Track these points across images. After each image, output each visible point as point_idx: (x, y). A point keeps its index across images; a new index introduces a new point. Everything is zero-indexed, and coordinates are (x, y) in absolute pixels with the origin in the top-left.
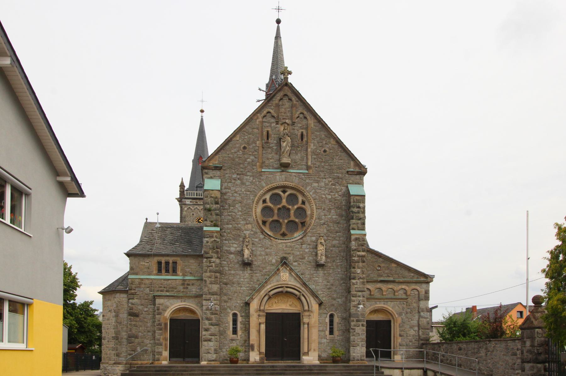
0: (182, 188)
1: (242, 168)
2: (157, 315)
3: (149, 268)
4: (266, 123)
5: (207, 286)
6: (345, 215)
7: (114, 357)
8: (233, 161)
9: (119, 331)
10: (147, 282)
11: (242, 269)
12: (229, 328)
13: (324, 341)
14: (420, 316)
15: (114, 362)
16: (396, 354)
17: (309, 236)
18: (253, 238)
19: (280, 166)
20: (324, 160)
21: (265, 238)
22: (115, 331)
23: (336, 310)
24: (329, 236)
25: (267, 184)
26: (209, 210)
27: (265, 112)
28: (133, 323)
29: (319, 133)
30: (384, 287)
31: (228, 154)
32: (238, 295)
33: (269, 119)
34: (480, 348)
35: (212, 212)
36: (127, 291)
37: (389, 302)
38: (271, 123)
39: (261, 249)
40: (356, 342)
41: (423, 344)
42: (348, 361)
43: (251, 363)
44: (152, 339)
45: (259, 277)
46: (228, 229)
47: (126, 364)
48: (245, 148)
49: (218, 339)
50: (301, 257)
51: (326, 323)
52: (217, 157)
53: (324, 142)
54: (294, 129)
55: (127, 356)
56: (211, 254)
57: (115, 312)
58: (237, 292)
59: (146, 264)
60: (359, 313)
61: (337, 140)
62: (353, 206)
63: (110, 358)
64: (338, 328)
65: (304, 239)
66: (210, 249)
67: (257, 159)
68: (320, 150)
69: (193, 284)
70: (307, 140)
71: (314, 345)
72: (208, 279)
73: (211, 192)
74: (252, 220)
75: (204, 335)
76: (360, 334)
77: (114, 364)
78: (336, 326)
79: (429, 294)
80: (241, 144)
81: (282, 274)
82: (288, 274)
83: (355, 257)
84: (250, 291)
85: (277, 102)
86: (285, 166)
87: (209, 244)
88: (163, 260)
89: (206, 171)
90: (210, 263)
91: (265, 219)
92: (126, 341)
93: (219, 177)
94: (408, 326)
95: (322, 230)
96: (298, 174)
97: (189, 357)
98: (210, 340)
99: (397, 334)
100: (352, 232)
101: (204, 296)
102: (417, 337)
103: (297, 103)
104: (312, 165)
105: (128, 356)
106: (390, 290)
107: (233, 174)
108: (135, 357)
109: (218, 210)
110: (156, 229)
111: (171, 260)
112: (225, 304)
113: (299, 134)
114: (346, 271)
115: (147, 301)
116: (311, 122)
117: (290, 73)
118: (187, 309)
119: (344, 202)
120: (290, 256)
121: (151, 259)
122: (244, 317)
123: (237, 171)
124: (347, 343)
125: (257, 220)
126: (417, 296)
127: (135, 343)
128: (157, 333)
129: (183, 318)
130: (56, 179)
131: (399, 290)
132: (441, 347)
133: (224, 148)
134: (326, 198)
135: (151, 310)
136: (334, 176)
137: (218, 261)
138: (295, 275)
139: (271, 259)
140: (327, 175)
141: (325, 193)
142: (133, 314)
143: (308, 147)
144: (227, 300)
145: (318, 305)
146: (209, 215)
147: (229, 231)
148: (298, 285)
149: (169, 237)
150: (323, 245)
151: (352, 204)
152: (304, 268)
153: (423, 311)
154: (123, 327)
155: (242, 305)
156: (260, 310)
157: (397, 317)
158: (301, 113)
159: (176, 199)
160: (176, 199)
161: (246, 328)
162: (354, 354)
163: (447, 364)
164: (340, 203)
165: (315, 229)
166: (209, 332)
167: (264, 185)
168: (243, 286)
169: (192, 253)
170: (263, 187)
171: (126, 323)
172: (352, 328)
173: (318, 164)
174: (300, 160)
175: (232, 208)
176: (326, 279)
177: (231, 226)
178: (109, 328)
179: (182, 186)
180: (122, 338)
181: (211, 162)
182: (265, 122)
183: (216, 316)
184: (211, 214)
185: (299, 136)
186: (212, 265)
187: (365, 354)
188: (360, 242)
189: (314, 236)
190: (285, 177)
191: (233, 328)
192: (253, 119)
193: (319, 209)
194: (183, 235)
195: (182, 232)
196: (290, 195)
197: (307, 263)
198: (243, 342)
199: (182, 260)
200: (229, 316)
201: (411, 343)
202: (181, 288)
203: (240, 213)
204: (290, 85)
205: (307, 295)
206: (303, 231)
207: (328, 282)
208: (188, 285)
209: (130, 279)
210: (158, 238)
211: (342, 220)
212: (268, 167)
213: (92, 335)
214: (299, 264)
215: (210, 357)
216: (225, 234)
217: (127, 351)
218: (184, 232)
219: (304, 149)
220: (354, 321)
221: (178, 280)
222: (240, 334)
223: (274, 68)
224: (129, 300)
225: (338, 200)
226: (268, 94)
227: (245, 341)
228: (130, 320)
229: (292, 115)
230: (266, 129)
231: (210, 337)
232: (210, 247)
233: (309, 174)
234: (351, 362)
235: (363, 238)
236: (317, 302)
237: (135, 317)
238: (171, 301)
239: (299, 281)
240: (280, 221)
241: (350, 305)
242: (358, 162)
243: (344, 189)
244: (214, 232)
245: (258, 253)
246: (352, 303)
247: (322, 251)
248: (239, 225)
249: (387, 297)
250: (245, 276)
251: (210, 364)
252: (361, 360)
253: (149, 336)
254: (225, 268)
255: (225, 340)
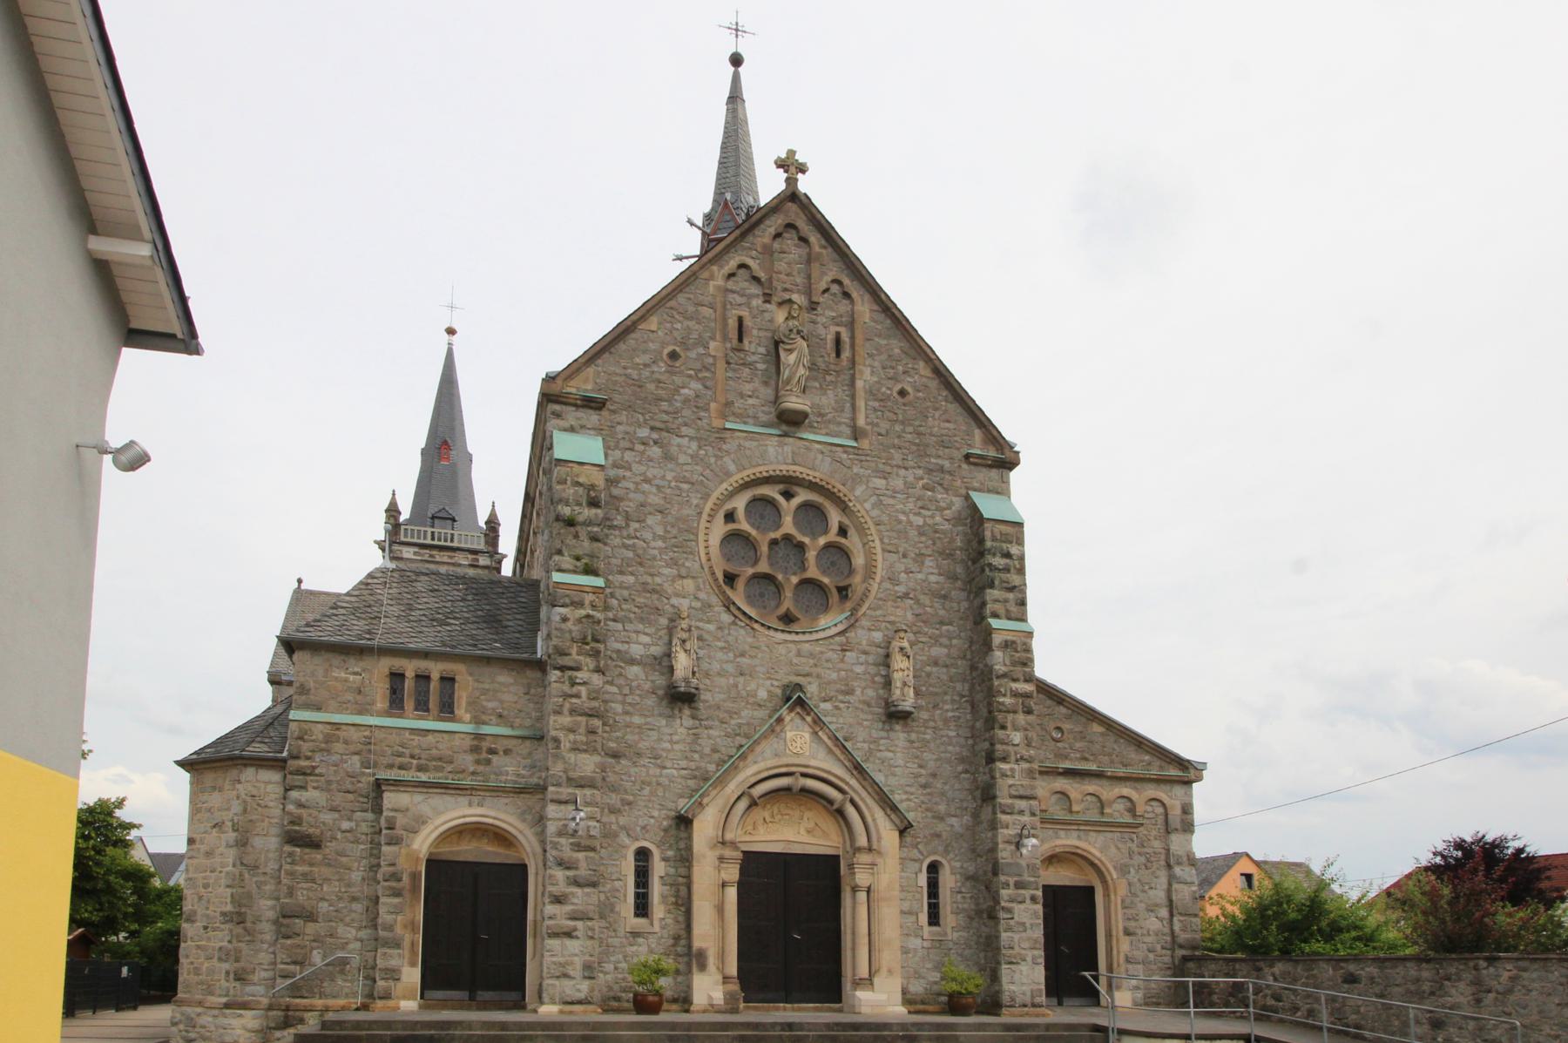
0: (393, 516)
1: (667, 413)
2: (389, 844)
3: (360, 692)
4: (735, 295)
5: (563, 758)
6: (963, 576)
7: (224, 984)
8: (639, 390)
9: (249, 895)
10: (355, 735)
11: (668, 711)
12: (625, 896)
13: (915, 943)
14: (1172, 879)
15: (224, 1000)
16: (1118, 988)
17: (863, 628)
18: (701, 620)
19: (776, 420)
20: (900, 417)
21: (736, 624)
22: (232, 895)
23: (946, 852)
24: (919, 632)
25: (741, 468)
26: (570, 523)
27: (732, 264)
28: (300, 869)
29: (884, 342)
30: (1074, 788)
31: (625, 368)
32: (653, 793)
33: (741, 282)
34: (1449, 979)
35: (578, 528)
36: (284, 761)
37: (1092, 834)
38: (750, 297)
39: (725, 657)
40: (1017, 949)
41: (1185, 959)
42: (993, 1005)
43: (698, 1012)
44: (364, 924)
45: (718, 740)
46: (621, 587)
47: (270, 1008)
48: (674, 356)
49: (596, 932)
50: (843, 688)
51: (919, 889)
52: (591, 370)
53: (900, 368)
54: (814, 322)
55: (275, 979)
56: (575, 656)
57: (234, 830)
58: (649, 784)
59: (351, 678)
60: (1023, 863)
61: (934, 365)
62: (993, 551)
63: (209, 986)
64: (955, 905)
65: (851, 635)
66: (573, 640)
67: (710, 393)
68: (888, 388)
69: (507, 752)
70: (854, 356)
71: (889, 957)
72: (566, 736)
73: (576, 468)
74: (697, 565)
75: (550, 918)
76: (1028, 925)
77: (227, 1006)
78: (948, 900)
79: (1192, 814)
80: (664, 344)
81: (789, 735)
82: (807, 736)
83: (1005, 695)
84: (691, 783)
85: (767, 240)
86: (791, 421)
87: (569, 625)
88: (410, 668)
89: (557, 407)
90: (573, 684)
91: (731, 569)
92: (274, 928)
93: (594, 429)
94: (1143, 905)
95: (899, 612)
96: (829, 448)
97: (488, 988)
98: (569, 934)
99: (1117, 927)
100: (995, 623)
101: (551, 789)
102: (1169, 938)
103: (824, 251)
104: (869, 428)
105: (279, 980)
106: (1089, 798)
107: (640, 426)
108: (302, 983)
109: (599, 525)
110: (381, 575)
111: (436, 669)
112: (613, 818)
113: (830, 338)
114: (972, 737)
115: (350, 796)
116: (864, 308)
117: (802, 169)
118: (486, 831)
119: (958, 539)
120: (810, 683)
121: (367, 662)
122: (672, 864)
123: (652, 418)
124: (990, 954)
125: (711, 567)
126: (1161, 819)
127: (306, 938)
128: (384, 904)
129: (471, 859)
130: (85, 242)
131: (1114, 801)
132: (1266, 970)
133: (612, 350)
134: (909, 522)
135: (364, 828)
136: (929, 462)
137: (597, 680)
138: (829, 738)
139: (752, 686)
140: (910, 458)
141: (907, 509)
142: (300, 839)
143: (857, 376)
144: (619, 805)
145: (897, 833)
146: (570, 537)
147: (625, 593)
148: (837, 770)
149: (425, 600)
150: (908, 657)
151: (989, 544)
152: (851, 720)
153: (1179, 864)
154: (265, 883)
155: (665, 823)
156: (723, 843)
157: (1115, 876)
158: (835, 281)
159: (376, 542)
160: (376, 542)
161: (677, 896)
162: (1013, 988)
163: (1297, 1024)
164: (949, 542)
165: (879, 608)
166: (568, 908)
167: (732, 468)
168: (668, 764)
169: (506, 654)
170: (728, 474)
171: (277, 867)
172: (1003, 908)
173: (884, 426)
174: (833, 408)
175: (637, 525)
176: (917, 757)
177: (631, 579)
178: (211, 881)
179: (392, 511)
180: (258, 920)
181: (572, 383)
182: (733, 292)
183: (592, 854)
184: (576, 536)
185: (830, 344)
186: (580, 692)
187: (1043, 987)
188: (1017, 655)
189: (878, 630)
190: (793, 453)
191: (637, 895)
192: (697, 278)
193: (890, 552)
194: (470, 598)
195: (466, 589)
196: (806, 506)
197: (861, 706)
198: (671, 942)
199: (471, 674)
200: (625, 857)
201: (1151, 956)
202: (467, 761)
203: (660, 543)
204: (805, 201)
205: (864, 802)
206: (843, 611)
207: (921, 766)
208: (492, 751)
209: (296, 723)
210: (390, 602)
211: (955, 589)
212: (742, 417)
213: (115, 901)
214: (837, 708)
215: (568, 992)
216: (614, 602)
217: (275, 963)
218: (474, 591)
219: (844, 380)
220: (1008, 885)
221: (457, 736)
222: (661, 915)
223: (728, 175)
224: (287, 790)
225: (944, 532)
226: (711, 241)
227: (677, 938)
228: (289, 860)
229: (810, 284)
230: (734, 312)
231: (571, 923)
232: (574, 635)
233: (860, 452)
234: (1004, 1010)
235: (1025, 644)
236: (896, 825)
237: (307, 850)
238: (438, 800)
239: (842, 757)
240: (776, 579)
241: (995, 836)
242: (995, 433)
243: (958, 503)
244: (587, 589)
245: (716, 666)
246: (1002, 830)
247: (906, 673)
248: (658, 580)
249: (1081, 817)
250: (676, 734)
251: (571, 1013)
252: (1034, 1005)
253: (353, 915)
254: (613, 705)
255: (613, 934)
